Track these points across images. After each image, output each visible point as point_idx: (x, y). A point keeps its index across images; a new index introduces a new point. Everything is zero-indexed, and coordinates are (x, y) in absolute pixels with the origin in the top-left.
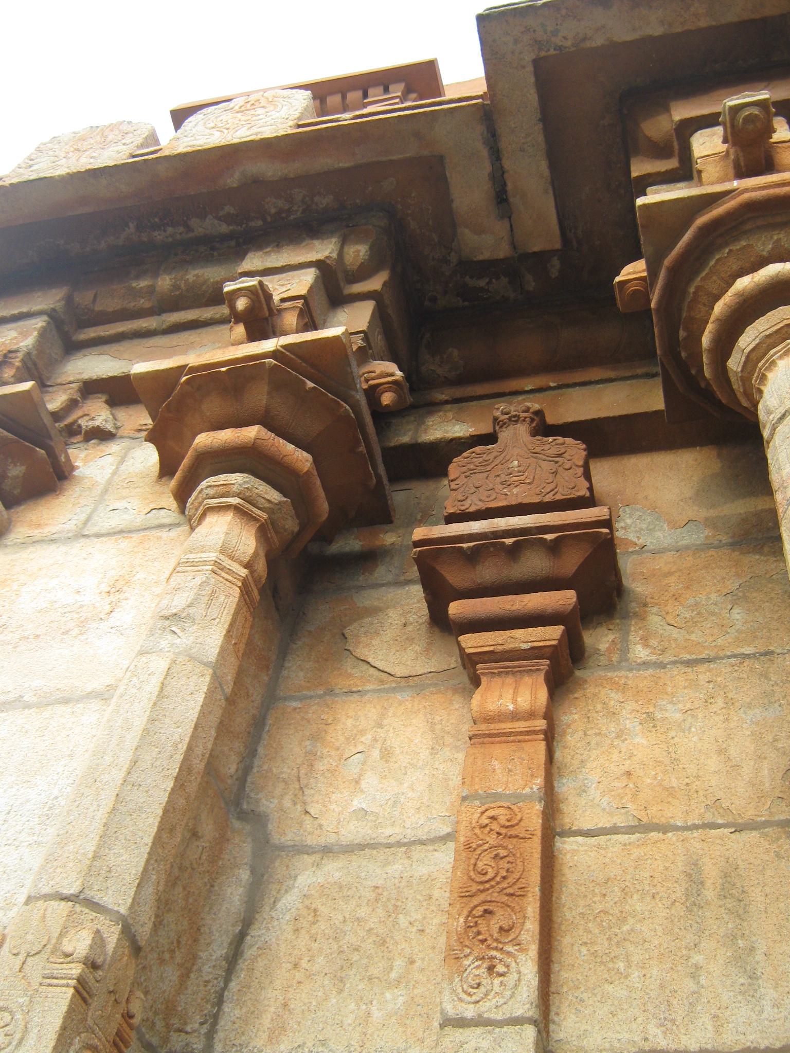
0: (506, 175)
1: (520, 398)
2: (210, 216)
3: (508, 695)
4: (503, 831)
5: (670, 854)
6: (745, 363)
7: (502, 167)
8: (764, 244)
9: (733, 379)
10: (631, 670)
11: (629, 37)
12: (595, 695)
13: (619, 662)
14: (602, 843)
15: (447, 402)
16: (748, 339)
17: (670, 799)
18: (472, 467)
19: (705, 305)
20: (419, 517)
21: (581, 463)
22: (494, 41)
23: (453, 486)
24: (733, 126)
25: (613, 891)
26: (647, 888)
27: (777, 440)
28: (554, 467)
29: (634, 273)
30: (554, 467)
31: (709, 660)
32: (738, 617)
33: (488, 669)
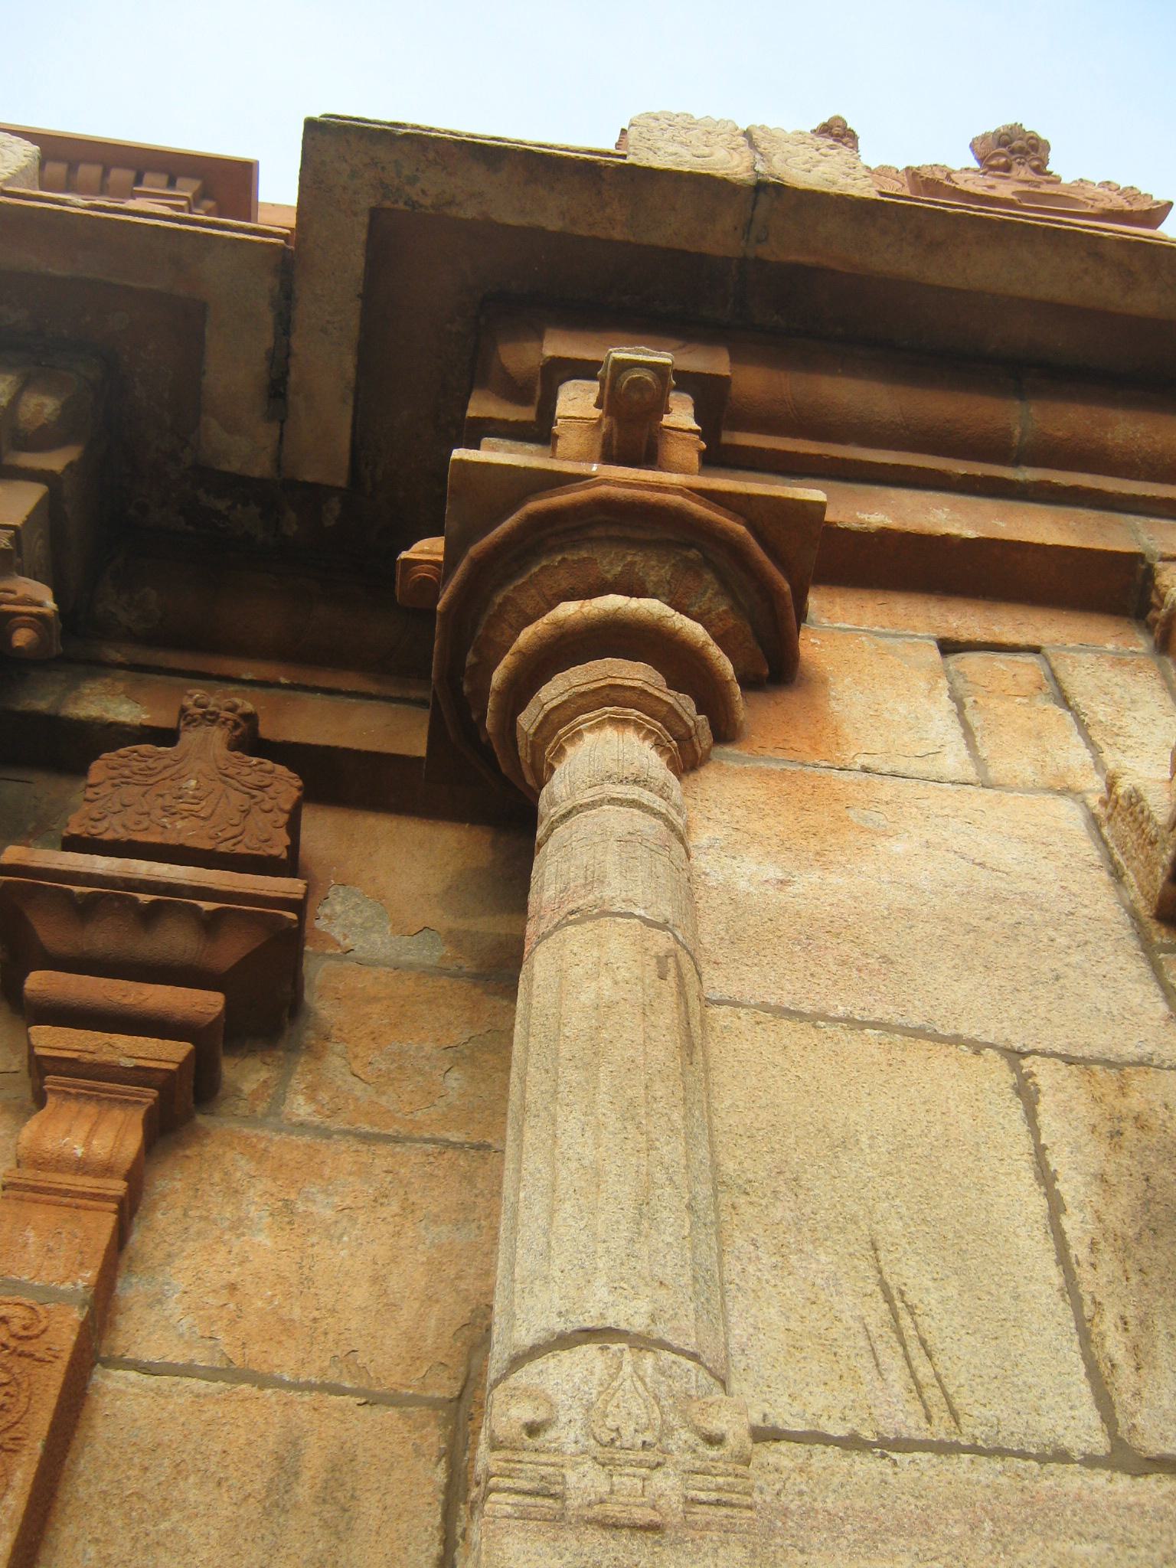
1: (232, 688)
3: (81, 1131)
4: (13, 1343)
5: (260, 1420)
6: (542, 723)
7: (288, 346)
8: (611, 563)
9: (521, 743)
10: (279, 1131)
11: (512, 220)
12: (216, 1157)
13: (265, 1116)
14: (165, 1387)
15: (120, 666)
16: (553, 692)
17: (284, 1338)
18: (127, 772)
20: (30, 827)
21: (288, 807)
23: (90, 794)
24: (613, 387)
25: (160, 1465)
26: (213, 1468)
27: (549, 848)
28: (248, 803)
29: (429, 552)
30: (248, 803)
31: (395, 1140)
32: (455, 1084)
33: (61, 1085)
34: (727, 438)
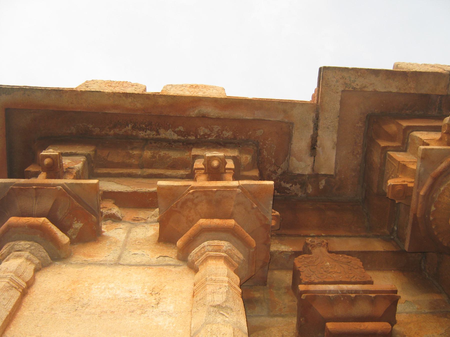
0: (318, 138)
2: (170, 130)
19: (447, 196)
22: (328, 79)
29: (398, 182)
34: (283, 184)
